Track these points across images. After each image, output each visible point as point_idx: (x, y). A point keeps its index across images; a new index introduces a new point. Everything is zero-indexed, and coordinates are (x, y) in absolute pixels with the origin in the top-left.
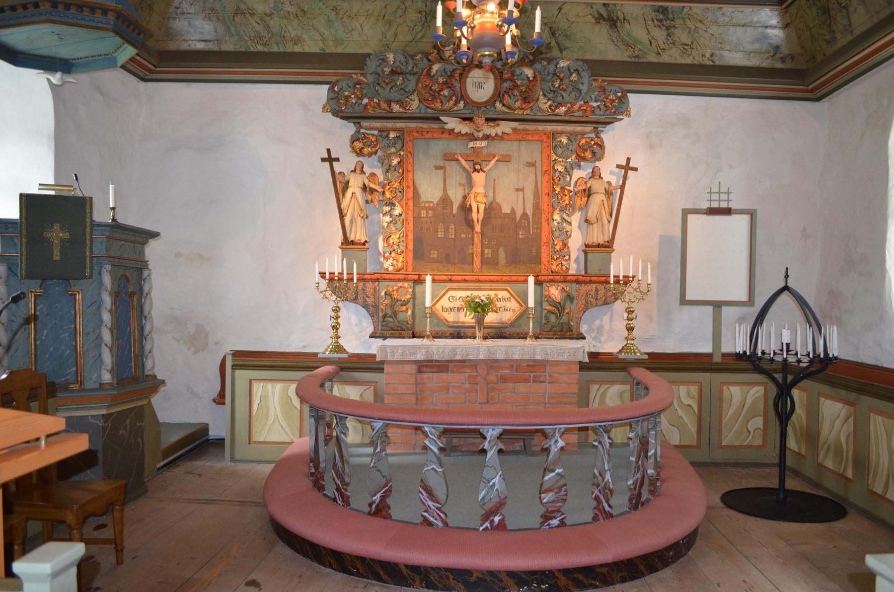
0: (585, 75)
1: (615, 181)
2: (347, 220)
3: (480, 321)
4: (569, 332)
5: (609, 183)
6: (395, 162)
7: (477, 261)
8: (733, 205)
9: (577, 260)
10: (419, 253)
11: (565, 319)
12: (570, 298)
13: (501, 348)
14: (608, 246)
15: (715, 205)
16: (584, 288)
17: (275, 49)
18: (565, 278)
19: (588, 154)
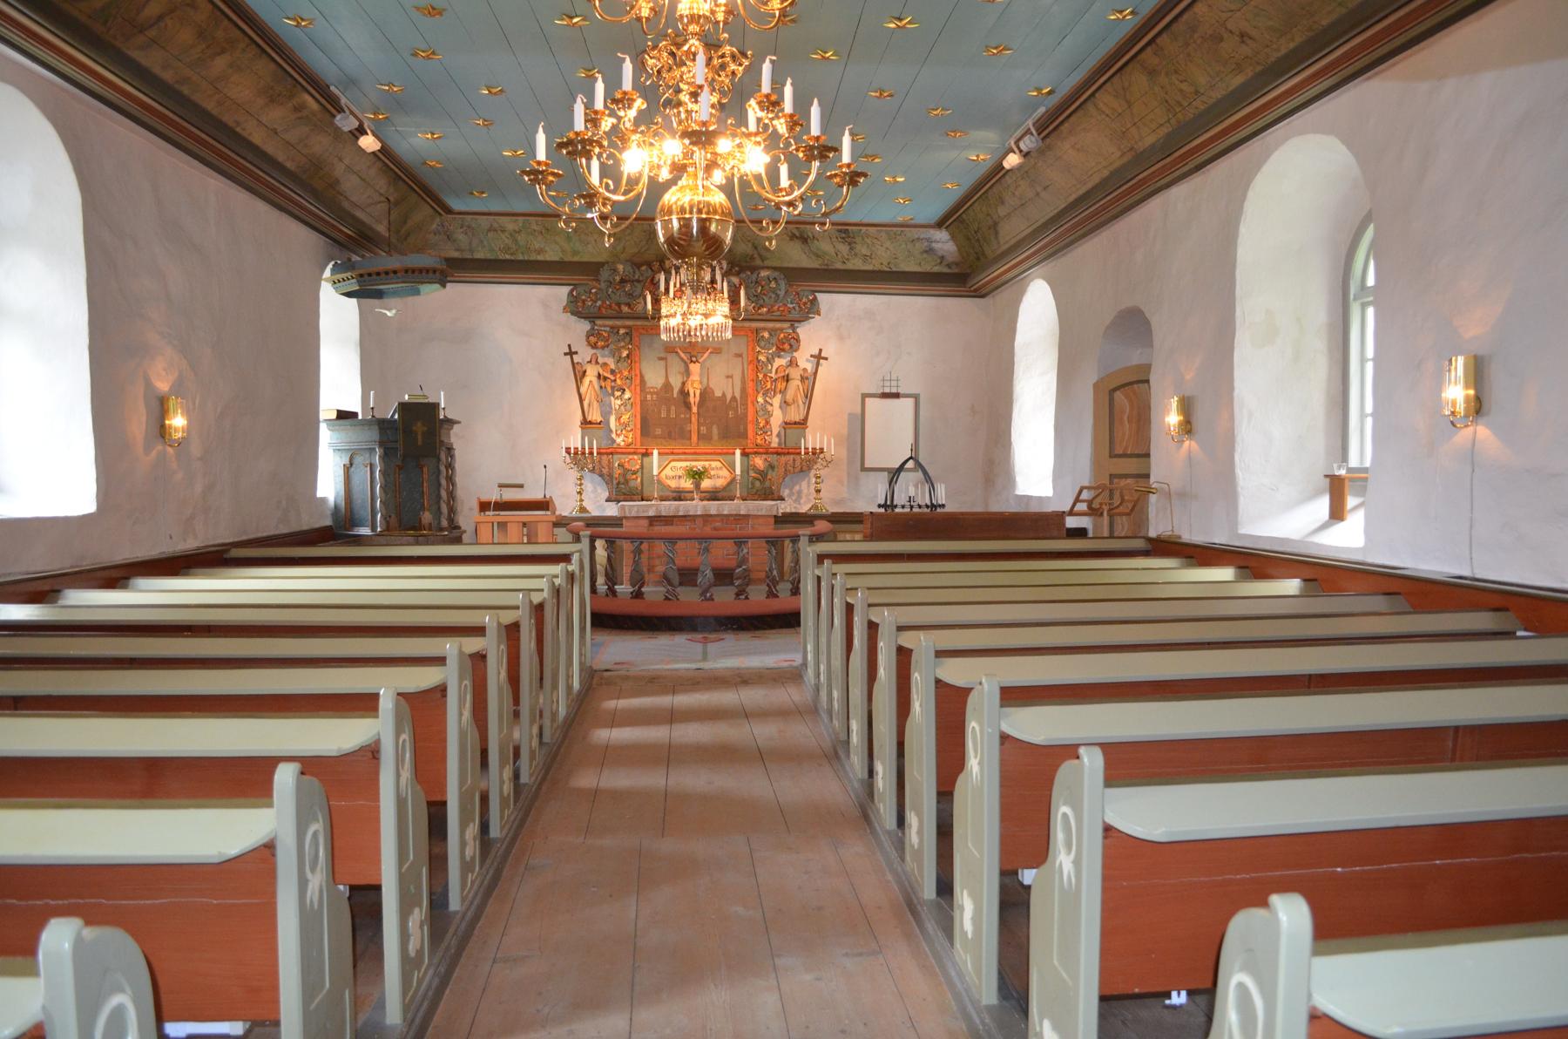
0: (783, 284)
1: (810, 367)
2: (586, 403)
3: (697, 486)
4: (769, 494)
5: (805, 370)
6: (625, 353)
7: (694, 437)
8: (901, 391)
9: (778, 435)
10: (646, 429)
11: (767, 484)
12: (772, 467)
13: (713, 507)
14: (803, 423)
15: (887, 390)
16: (783, 458)
17: (521, 257)
18: (767, 451)
19: (786, 346)
